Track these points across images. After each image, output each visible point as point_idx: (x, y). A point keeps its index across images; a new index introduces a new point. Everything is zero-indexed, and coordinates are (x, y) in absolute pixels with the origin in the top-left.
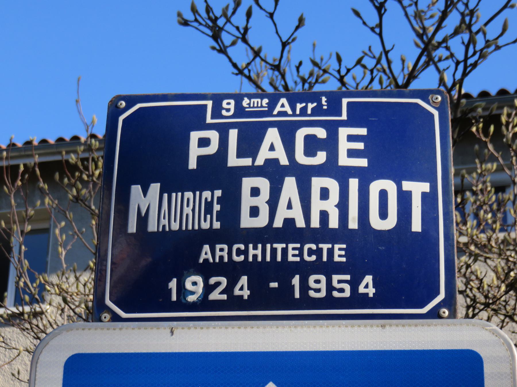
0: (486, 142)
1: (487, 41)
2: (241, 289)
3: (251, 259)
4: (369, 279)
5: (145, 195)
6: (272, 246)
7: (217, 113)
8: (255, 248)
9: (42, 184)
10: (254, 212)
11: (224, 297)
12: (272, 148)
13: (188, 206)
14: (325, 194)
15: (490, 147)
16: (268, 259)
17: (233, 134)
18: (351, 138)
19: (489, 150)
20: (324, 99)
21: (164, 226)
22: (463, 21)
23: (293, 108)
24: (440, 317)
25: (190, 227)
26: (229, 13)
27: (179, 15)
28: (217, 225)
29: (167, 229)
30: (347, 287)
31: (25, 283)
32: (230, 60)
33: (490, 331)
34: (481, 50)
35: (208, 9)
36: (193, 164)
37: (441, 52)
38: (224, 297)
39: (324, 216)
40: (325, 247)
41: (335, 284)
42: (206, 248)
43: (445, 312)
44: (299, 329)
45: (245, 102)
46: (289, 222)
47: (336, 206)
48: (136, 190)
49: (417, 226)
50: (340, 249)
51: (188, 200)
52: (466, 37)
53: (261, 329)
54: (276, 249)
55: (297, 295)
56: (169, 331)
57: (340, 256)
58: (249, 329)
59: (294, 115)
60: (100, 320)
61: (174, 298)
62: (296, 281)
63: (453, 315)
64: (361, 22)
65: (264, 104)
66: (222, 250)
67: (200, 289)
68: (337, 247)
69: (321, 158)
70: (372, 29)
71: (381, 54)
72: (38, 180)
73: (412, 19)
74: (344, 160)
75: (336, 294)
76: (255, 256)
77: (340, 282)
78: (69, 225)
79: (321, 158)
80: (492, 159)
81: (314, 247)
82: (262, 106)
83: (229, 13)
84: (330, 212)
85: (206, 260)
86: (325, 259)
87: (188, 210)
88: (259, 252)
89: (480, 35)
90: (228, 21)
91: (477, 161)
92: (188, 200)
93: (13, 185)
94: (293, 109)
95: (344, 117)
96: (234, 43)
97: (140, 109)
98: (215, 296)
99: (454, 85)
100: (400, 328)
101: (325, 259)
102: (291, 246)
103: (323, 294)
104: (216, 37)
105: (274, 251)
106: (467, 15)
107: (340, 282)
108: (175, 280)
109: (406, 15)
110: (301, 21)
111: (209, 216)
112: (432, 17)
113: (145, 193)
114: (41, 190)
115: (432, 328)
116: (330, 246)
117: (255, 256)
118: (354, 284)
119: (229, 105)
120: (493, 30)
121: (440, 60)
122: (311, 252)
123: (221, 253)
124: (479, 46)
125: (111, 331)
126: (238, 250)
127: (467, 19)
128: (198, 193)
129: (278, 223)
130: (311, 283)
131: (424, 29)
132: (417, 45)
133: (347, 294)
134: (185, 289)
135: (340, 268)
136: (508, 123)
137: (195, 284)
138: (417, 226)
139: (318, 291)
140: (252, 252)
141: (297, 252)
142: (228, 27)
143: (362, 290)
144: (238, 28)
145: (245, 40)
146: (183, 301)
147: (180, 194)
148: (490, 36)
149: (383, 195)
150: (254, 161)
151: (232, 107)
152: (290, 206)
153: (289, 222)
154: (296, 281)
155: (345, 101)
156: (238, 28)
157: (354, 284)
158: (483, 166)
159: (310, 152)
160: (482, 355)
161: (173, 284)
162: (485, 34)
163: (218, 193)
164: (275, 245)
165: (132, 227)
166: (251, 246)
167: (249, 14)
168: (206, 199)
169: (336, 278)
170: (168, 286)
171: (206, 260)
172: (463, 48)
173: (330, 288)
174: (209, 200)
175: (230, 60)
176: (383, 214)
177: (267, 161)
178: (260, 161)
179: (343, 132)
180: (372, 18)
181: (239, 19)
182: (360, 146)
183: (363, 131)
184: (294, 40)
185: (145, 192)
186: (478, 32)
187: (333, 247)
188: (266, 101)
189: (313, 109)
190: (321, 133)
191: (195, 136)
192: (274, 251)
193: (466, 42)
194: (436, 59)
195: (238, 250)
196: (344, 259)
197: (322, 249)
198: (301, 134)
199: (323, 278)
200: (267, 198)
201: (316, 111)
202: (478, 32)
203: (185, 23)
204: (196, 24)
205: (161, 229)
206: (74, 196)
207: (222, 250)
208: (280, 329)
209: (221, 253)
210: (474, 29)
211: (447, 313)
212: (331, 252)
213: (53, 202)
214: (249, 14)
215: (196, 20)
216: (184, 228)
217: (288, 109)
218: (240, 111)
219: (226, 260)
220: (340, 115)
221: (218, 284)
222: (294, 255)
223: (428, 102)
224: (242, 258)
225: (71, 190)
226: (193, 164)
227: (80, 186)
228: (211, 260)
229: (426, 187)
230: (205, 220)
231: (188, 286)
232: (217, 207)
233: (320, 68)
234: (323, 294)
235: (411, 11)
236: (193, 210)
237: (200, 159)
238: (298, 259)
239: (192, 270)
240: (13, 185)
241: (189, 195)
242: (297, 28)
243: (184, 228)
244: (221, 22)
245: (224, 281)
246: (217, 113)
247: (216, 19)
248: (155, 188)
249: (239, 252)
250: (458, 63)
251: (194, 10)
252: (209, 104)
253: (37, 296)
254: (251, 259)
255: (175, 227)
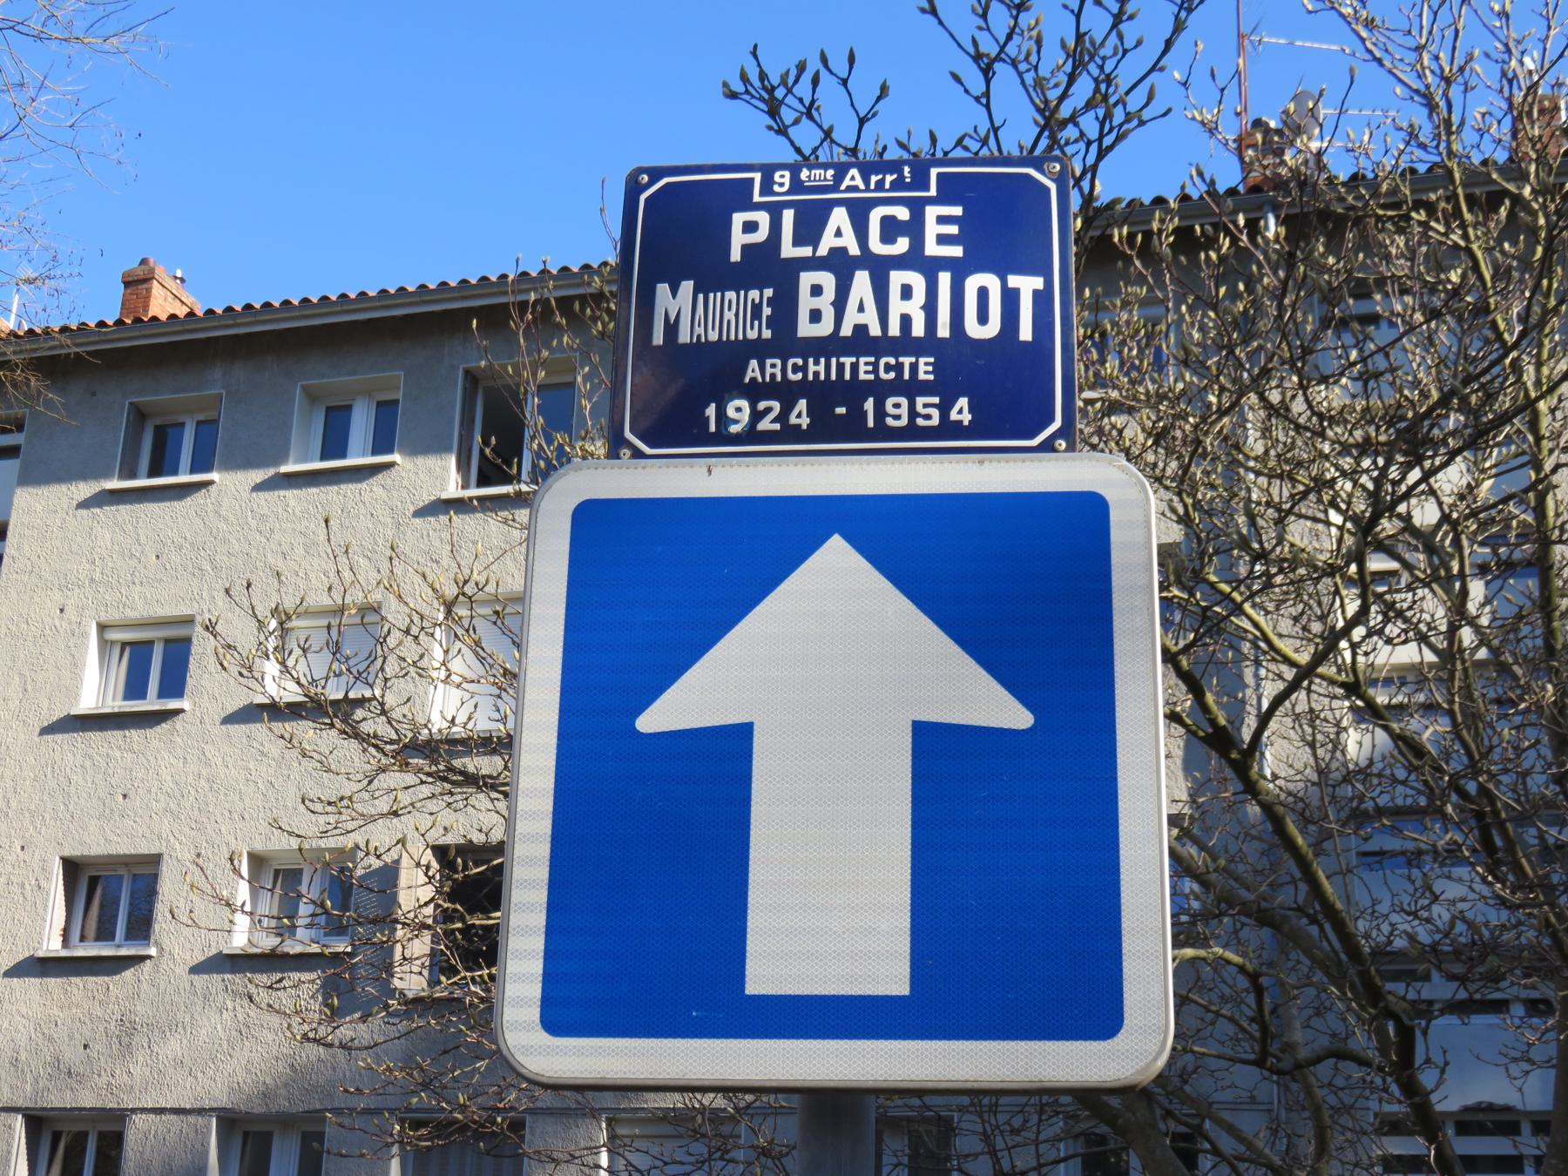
0: (1131, 256)
1: (1127, 114)
2: (799, 416)
3: (811, 377)
4: (963, 402)
5: (674, 297)
6: (838, 361)
7: (767, 188)
8: (817, 363)
9: (558, 319)
10: (816, 316)
11: (777, 426)
12: (838, 233)
13: (729, 309)
14: (907, 292)
15: (1138, 263)
16: (833, 377)
17: (788, 216)
18: (942, 220)
19: (1136, 267)
20: (907, 169)
21: (699, 336)
22: (1097, 90)
23: (867, 181)
24: (1054, 450)
25: (733, 337)
26: (791, 81)
27: (725, 85)
28: (767, 334)
29: (703, 340)
30: (935, 413)
31: (539, 445)
32: (792, 143)
33: (1119, 467)
34: (1121, 125)
35: (763, 76)
36: (736, 256)
37: (1070, 132)
38: (777, 426)
39: (906, 320)
40: (907, 361)
41: (920, 409)
42: (754, 363)
43: (1062, 444)
44: (872, 466)
45: (804, 174)
46: (861, 329)
47: (922, 308)
48: (663, 289)
49: (1026, 333)
50: (926, 364)
51: (730, 302)
52: (1101, 112)
53: (824, 467)
54: (843, 364)
55: (871, 424)
56: (706, 469)
57: (926, 373)
58: (808, 467)
59: (868, 189)
60: (618, 457)
61: (713, 428)
62: (869, 405)
63: (1071, 448)
64: (936, 21)
65: (829, 177)
66: (773, 366)
67: (745, 416)
68: (922, 360)
69: (902, 245)
70: (977, 99)
71: (989, 130)
72: (553, 313)
73: (1031, 89)
74: (932, 249)
75: (920, 422)
76: (816, 374)
77: (925, 406)
78: (594, 368)
79: (902, 245)
80: (1141, 280)
81: (892, 361)
82: (825, 179)
83: (791, 81)
84: (913, 316)
85: (753, 380)
86: (906, 376)
87: (729, 315)
88: (821, 368)
89: (1120, 107)
90: (789, 91)
91: (1122, 283)
92: (730, 302)
93: (522, 320)
94: (867, 182)
95: (933, 192)
96: (797, 122)
97: (667, 184)
98: (765, 425)
99: (1084, 173)
100: (1003, 464)
101: (906, 376)
102: (862, 360)
103: (904, 422)
104: (773, 112)
105: (841, 367)
106: (1103, 81)
107: (925, 406)
108: (713, 405)
109: (1023, 82)
110: (884, 90)
111: (756, 323)
112: (1056, 86)
113: (674, 294)
114: (559, 325)
115: (1044, 463)
116: (913, 360)
117: (816, 374)
118: (944, 409)
119: (783, 178)
120: (1134, 102)
121: (1067, 143)
122: (888, 368)
123: (773, 370)
124: (1116, 122)
125: (631, 470)
126: (795, 365)
127: (1103, 87)
128: (742, 293)
129: (846, 331)
130: (889, 408)
131: (1046, 102)
132: (1036, 123)
133: (935, 421)
134: (727, 417)
135: (926, 389)
136: (1160, 231)
137: (739, 410)
138: (1026, 333)
139: (897, 417)
140: (812, 368)
141: (870, 368)
142: (790, 100)
143: (954, 416)
144: (801, 100)
145: (811, 117)
146: (724, 432)
147: (719, 294)
148: (1131, 108)
149: (983, 293)
150: (815, 251)
151: (787, 180)
152: (861, 309)
153: (861, 329)
154: (869, 405)
155: (934, 172)
156: (801, 100)
157: (944, 409)
158: (1129, 289)
159: (888, 237)
160: (1108, 498)
161: (711, 411)
162: (1125, 105)
163: (769, 292)
164: (842, 360)
165: (658, 338)
166: (811, 360)
167: (815, 81)
168: (753, 300)
169: (920, 401)
170: (704, 413)
171: (753, 380)
172: (1097, 126)
173: (913, 414)
174: (757, 301)
175: (792, 143)
176: (983, 318)
177: (833, 251)
178: (823, 251)
179: (932, 212)
180: (977, 85)
181: (803, 89)
182: (953, 230)
183: (957, 211)
184: (874, 115)
185: (674, 292)
186: (1116, 104)
187: (917, 361)
188: (830, 172)
189: (892, 182)
190: (902, 213)
191: (738, 219)
192: (841, 367)
193: (1101, 117)
194: (1063, 142)
195: (795, 365)
196: (931, 377)
197: (902, 364)
198: (876, 215)
199: (904, 401)
200: (832, 297)
201: (896, 186)
202: (1116, 104)
203: (733, 96)
204: (747, 97)
205: (695, 340)
206: (598, 332)
207: (773, 366)
208: (848, 466)
209: (773, 370)
210: (1112, 100)
211: (1064, 445)
212: (914, 367)
213: (573, 342)
214: (815, 81)
215: (747, 92)
216: (725, 338)
217: (859, 182)
218: (797, 186)
219: (779, 378)
220: (927, 189)
221: (769, 410)
222: (866, 372)
223: (1042, 172)
224: (799, 376)
225: (596, 325)
226: (736, 256)
227: (607, 319)
228: (760, 380)
229: (1038, 283)
230: (752, 328)
231: (731, 412)
232: (767, 311)
233: (908, 151)
234: (904, 422)
235: (1029, 78)
236: (737, 315)
237: (746, 248)
238: (871, 377)
239: (735, 393)
240: (522, 320)
241: (731, 295)
242: (879, 99)
243: (725, 338)
244: (780, 93)
245: (776, 406)
246: (767, 188)
247: (774, 88)
248: (687, 286)
249: (796, 369)
250: (1089, 143)
251: (744, 78)
252: (757, 177)
253: (555, 462)
254: (811, 377)
255: (713, 336)
